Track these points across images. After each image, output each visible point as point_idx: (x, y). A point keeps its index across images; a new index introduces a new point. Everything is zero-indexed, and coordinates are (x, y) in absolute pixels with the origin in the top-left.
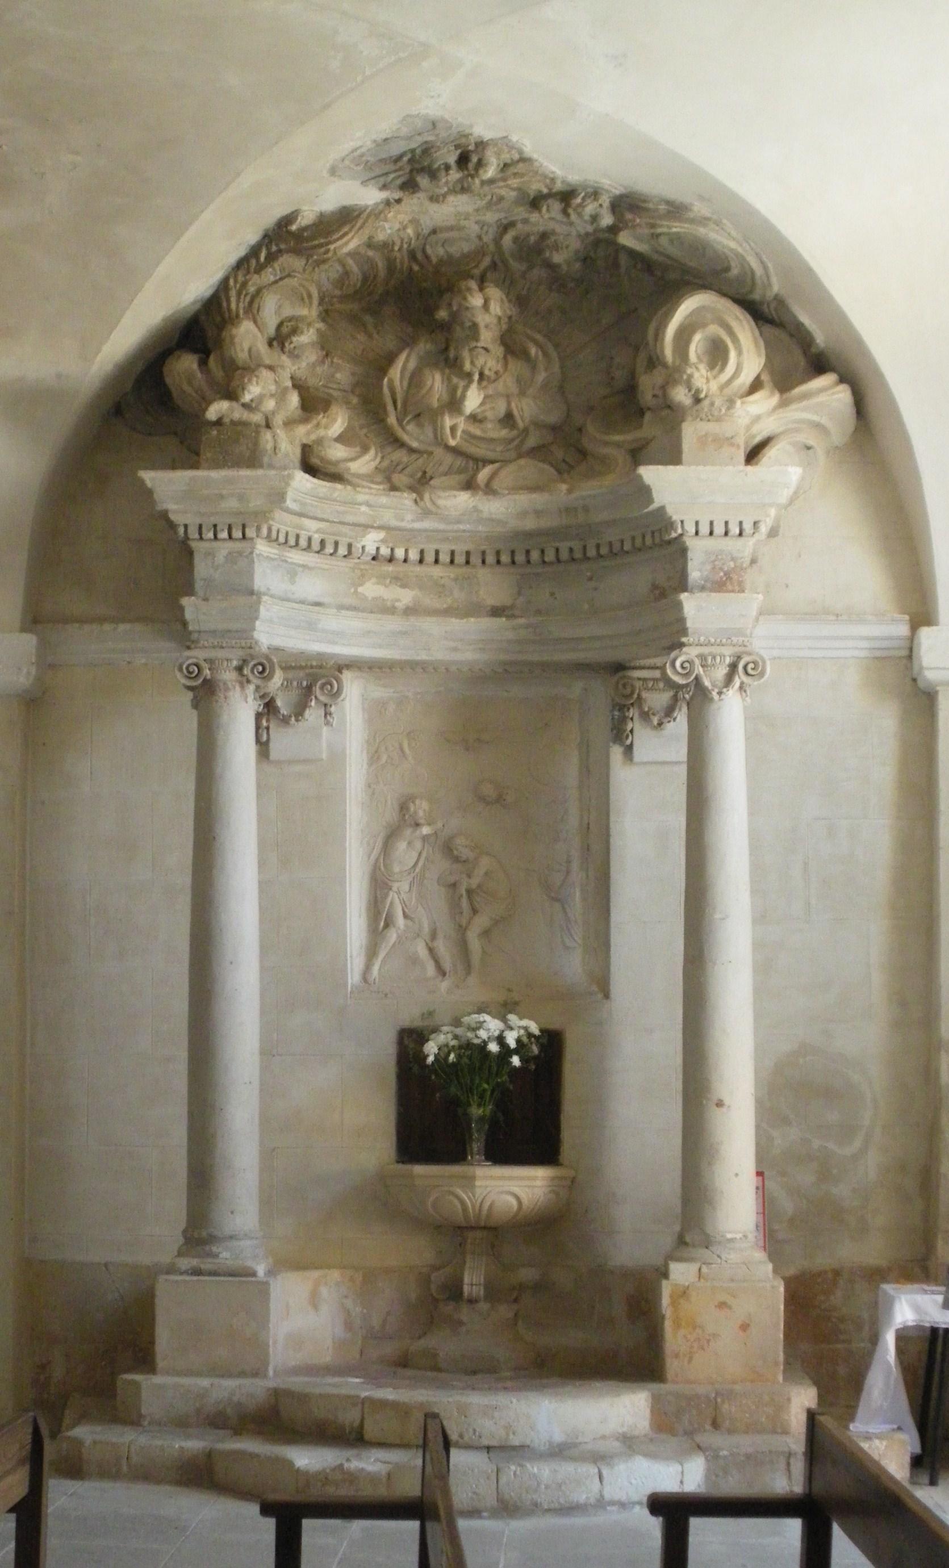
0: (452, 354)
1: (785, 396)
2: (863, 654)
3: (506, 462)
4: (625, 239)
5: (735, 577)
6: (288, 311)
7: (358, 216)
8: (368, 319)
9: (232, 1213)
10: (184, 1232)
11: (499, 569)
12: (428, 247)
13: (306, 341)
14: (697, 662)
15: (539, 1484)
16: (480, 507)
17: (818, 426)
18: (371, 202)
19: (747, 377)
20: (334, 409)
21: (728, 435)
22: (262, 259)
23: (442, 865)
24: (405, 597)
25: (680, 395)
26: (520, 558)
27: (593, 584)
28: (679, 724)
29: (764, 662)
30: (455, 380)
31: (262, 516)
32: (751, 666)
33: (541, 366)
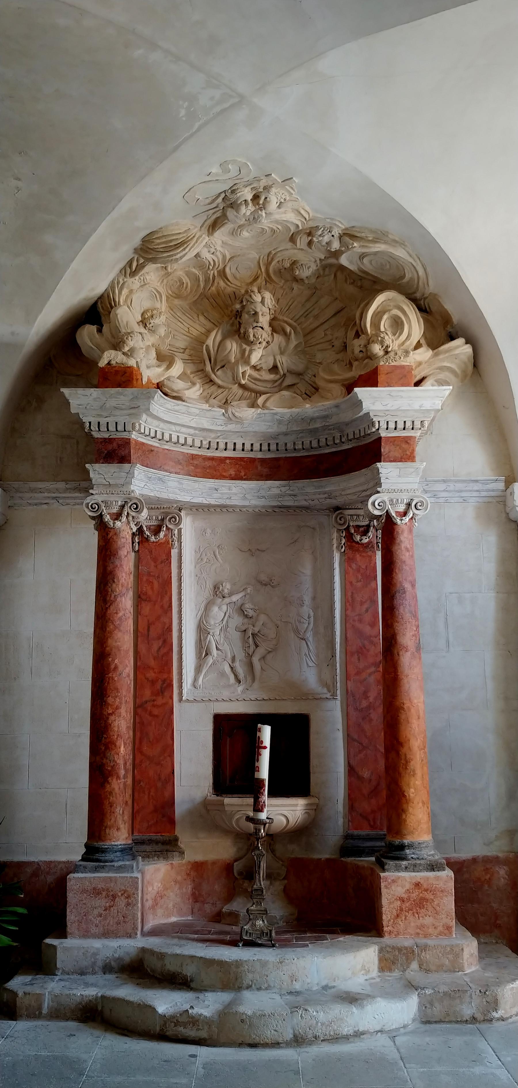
1: (435, 351)
4: (344, 260)
14: (388, 503)
15: (317, 1023)
23: (237, 620)
30: (244, 346)
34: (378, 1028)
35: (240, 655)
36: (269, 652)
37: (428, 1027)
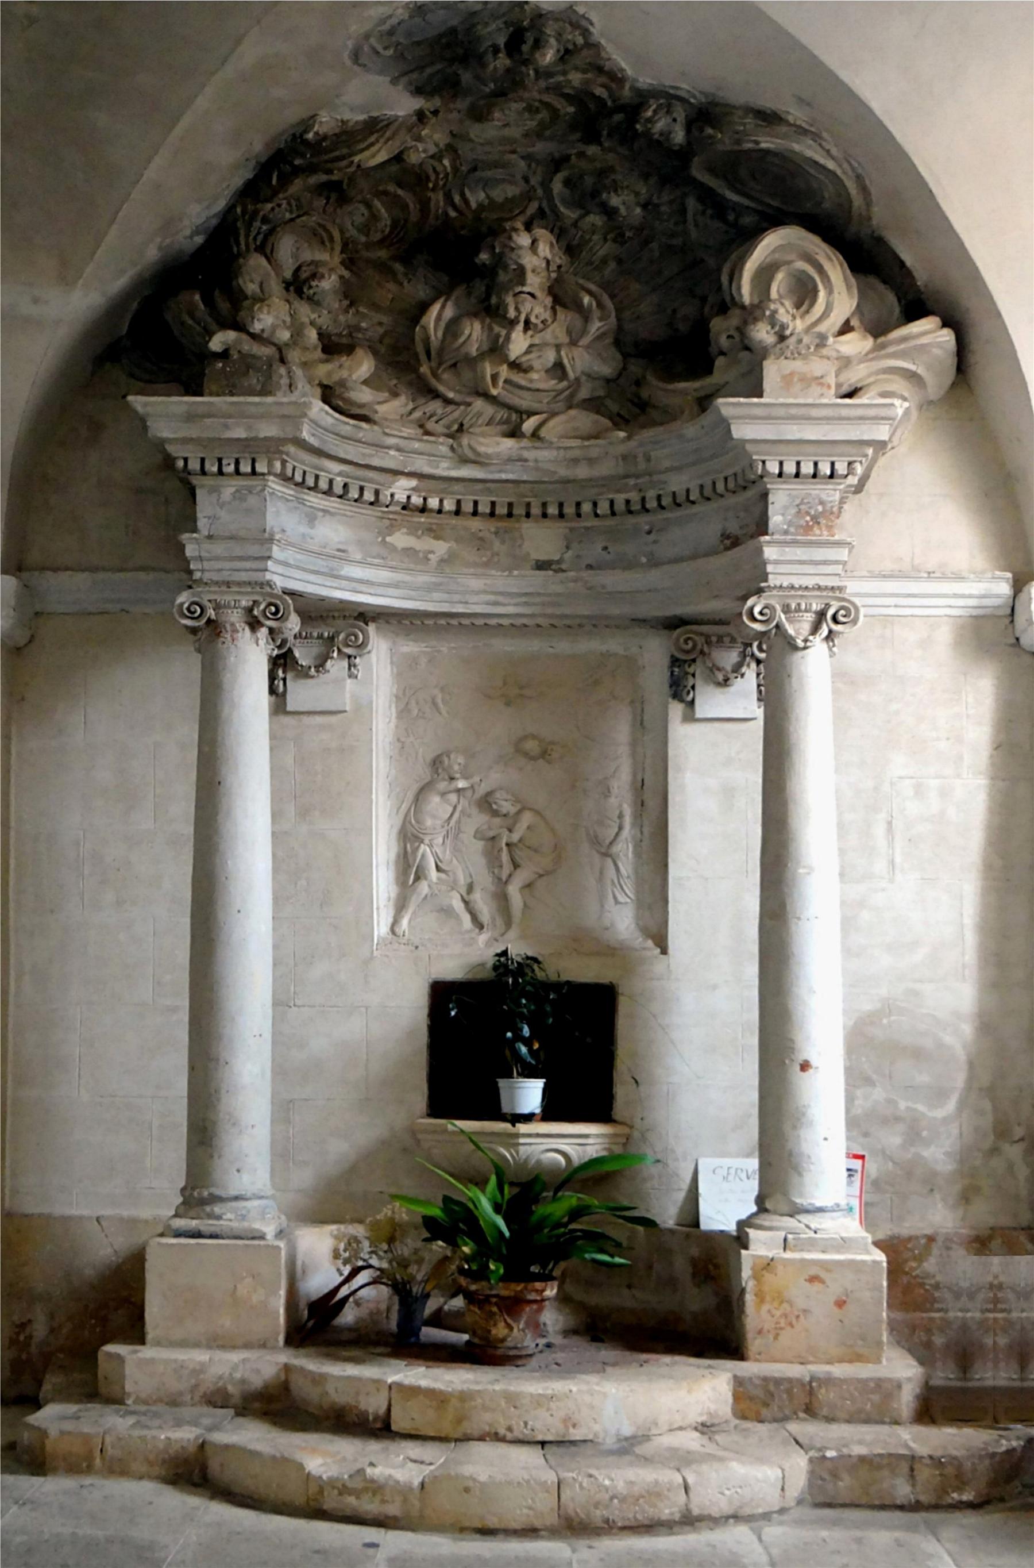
0: (494, 300)
3: (553, 414)
5: (823, 521)
6: (307, 255)
7: (387, 126)
8: (398, 267)
9: (238, 1171)
10: (183, 1190)
11: (547, 523)
13: (327, 288)
14: (778, 608)
16: (526, 454)
19: (836, 319)
20: (360, 352)
23: (479, 820)
24: (441, 548)
25: (762, 333)
26: (569, 510)
27: (652, 537)
28: (749, 680)
30: (497, 329)
32: (842, 612)
34: (731, 1512)
35: (484, 880)
36: (541, 876)
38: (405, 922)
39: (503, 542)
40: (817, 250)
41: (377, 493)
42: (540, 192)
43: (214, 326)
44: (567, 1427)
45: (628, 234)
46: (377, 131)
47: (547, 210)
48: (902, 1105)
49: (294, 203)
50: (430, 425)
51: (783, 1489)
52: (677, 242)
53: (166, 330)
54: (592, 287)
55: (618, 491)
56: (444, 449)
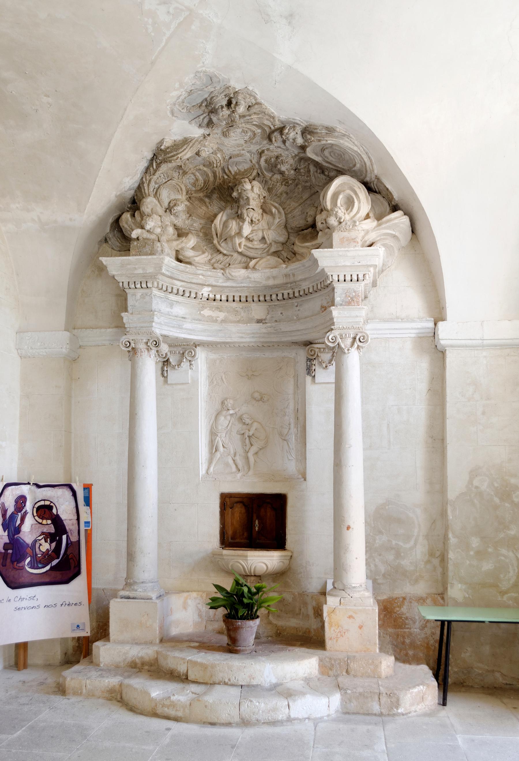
0: (239, 213)
2: (413, 335)
3: (262, 258)
5: (355, 299)
6: (173, 197)
8: (207, 200)
11: (260, 303)
12: (229, 167)
14: (338, 337)
15: (259, 711)
16: (250, 276)
17: (394, 236)
18: (196, 136)
20: (190, 236)
21: (353, 237)
22: (155, 167)
23: (239, 426)
24: (222, 315)
25: (333, 221)
26: (268, 298)
27: (298, 308)
28: (332, 368)
29: (368, 336)
31: (153, 277)
33: (277, 216)
35: (240, 451)
37: (347, 716)
38: (212, 469)
39: (245, 312)
40: (355, 185)
41: (196, 293)
42: (257, 166)
43: (134, 227)
44: (250, 679)
45: (290, 182)
46: (187, 144)
47: (260, 173)
48: (394, 542)
49: (166, 175)
50: (216, 265)
51: (329, 706)
52: (308, 184)
53: (120, 229)
54: (276, 205)
55: (285, 290)
56: (220, 275)
